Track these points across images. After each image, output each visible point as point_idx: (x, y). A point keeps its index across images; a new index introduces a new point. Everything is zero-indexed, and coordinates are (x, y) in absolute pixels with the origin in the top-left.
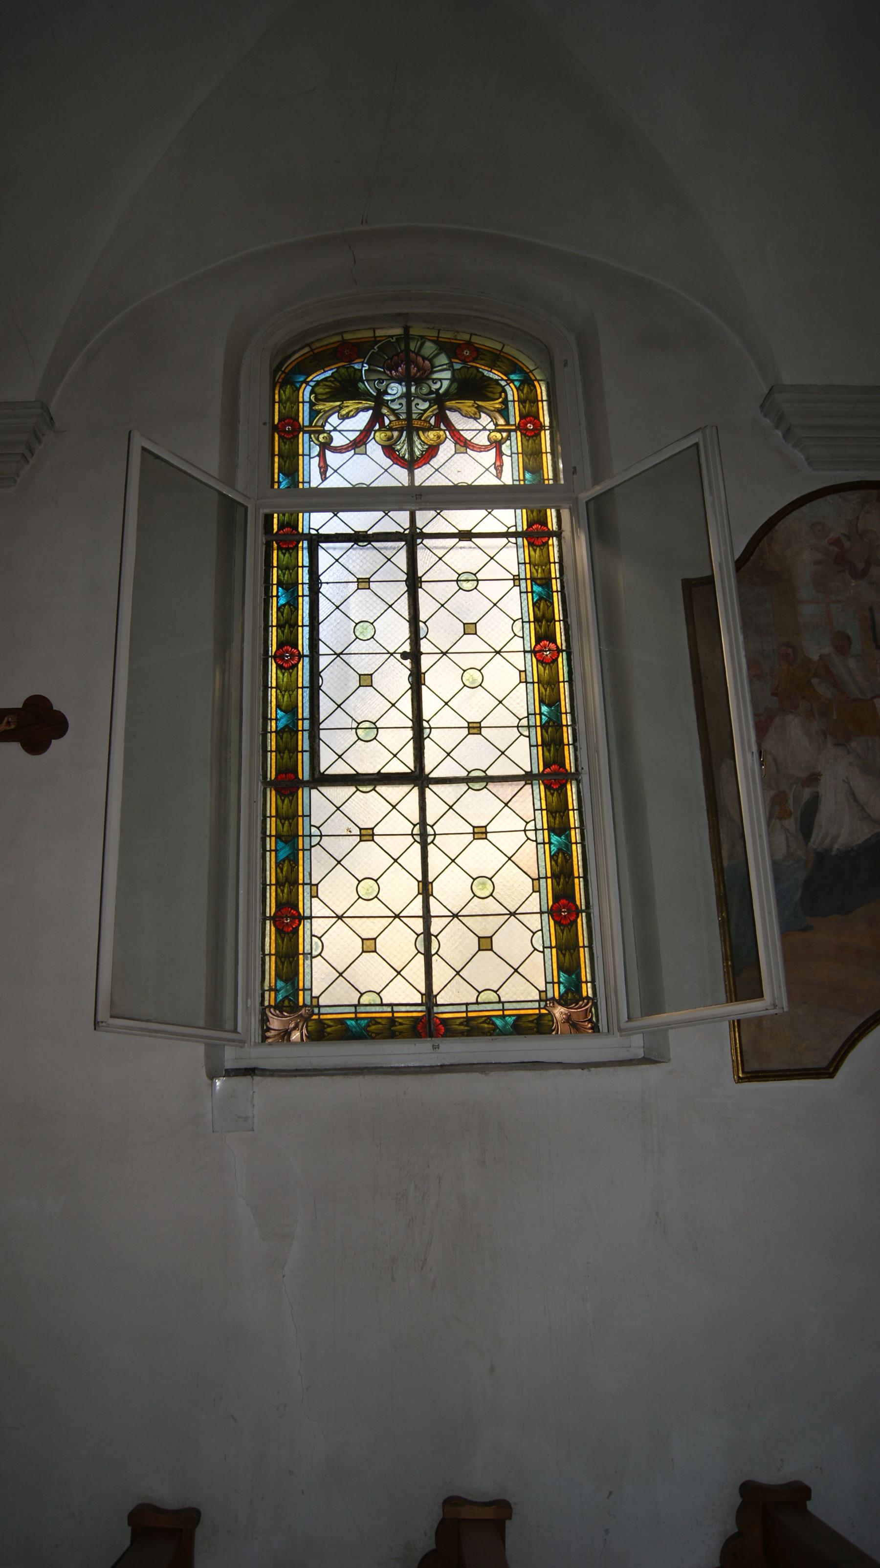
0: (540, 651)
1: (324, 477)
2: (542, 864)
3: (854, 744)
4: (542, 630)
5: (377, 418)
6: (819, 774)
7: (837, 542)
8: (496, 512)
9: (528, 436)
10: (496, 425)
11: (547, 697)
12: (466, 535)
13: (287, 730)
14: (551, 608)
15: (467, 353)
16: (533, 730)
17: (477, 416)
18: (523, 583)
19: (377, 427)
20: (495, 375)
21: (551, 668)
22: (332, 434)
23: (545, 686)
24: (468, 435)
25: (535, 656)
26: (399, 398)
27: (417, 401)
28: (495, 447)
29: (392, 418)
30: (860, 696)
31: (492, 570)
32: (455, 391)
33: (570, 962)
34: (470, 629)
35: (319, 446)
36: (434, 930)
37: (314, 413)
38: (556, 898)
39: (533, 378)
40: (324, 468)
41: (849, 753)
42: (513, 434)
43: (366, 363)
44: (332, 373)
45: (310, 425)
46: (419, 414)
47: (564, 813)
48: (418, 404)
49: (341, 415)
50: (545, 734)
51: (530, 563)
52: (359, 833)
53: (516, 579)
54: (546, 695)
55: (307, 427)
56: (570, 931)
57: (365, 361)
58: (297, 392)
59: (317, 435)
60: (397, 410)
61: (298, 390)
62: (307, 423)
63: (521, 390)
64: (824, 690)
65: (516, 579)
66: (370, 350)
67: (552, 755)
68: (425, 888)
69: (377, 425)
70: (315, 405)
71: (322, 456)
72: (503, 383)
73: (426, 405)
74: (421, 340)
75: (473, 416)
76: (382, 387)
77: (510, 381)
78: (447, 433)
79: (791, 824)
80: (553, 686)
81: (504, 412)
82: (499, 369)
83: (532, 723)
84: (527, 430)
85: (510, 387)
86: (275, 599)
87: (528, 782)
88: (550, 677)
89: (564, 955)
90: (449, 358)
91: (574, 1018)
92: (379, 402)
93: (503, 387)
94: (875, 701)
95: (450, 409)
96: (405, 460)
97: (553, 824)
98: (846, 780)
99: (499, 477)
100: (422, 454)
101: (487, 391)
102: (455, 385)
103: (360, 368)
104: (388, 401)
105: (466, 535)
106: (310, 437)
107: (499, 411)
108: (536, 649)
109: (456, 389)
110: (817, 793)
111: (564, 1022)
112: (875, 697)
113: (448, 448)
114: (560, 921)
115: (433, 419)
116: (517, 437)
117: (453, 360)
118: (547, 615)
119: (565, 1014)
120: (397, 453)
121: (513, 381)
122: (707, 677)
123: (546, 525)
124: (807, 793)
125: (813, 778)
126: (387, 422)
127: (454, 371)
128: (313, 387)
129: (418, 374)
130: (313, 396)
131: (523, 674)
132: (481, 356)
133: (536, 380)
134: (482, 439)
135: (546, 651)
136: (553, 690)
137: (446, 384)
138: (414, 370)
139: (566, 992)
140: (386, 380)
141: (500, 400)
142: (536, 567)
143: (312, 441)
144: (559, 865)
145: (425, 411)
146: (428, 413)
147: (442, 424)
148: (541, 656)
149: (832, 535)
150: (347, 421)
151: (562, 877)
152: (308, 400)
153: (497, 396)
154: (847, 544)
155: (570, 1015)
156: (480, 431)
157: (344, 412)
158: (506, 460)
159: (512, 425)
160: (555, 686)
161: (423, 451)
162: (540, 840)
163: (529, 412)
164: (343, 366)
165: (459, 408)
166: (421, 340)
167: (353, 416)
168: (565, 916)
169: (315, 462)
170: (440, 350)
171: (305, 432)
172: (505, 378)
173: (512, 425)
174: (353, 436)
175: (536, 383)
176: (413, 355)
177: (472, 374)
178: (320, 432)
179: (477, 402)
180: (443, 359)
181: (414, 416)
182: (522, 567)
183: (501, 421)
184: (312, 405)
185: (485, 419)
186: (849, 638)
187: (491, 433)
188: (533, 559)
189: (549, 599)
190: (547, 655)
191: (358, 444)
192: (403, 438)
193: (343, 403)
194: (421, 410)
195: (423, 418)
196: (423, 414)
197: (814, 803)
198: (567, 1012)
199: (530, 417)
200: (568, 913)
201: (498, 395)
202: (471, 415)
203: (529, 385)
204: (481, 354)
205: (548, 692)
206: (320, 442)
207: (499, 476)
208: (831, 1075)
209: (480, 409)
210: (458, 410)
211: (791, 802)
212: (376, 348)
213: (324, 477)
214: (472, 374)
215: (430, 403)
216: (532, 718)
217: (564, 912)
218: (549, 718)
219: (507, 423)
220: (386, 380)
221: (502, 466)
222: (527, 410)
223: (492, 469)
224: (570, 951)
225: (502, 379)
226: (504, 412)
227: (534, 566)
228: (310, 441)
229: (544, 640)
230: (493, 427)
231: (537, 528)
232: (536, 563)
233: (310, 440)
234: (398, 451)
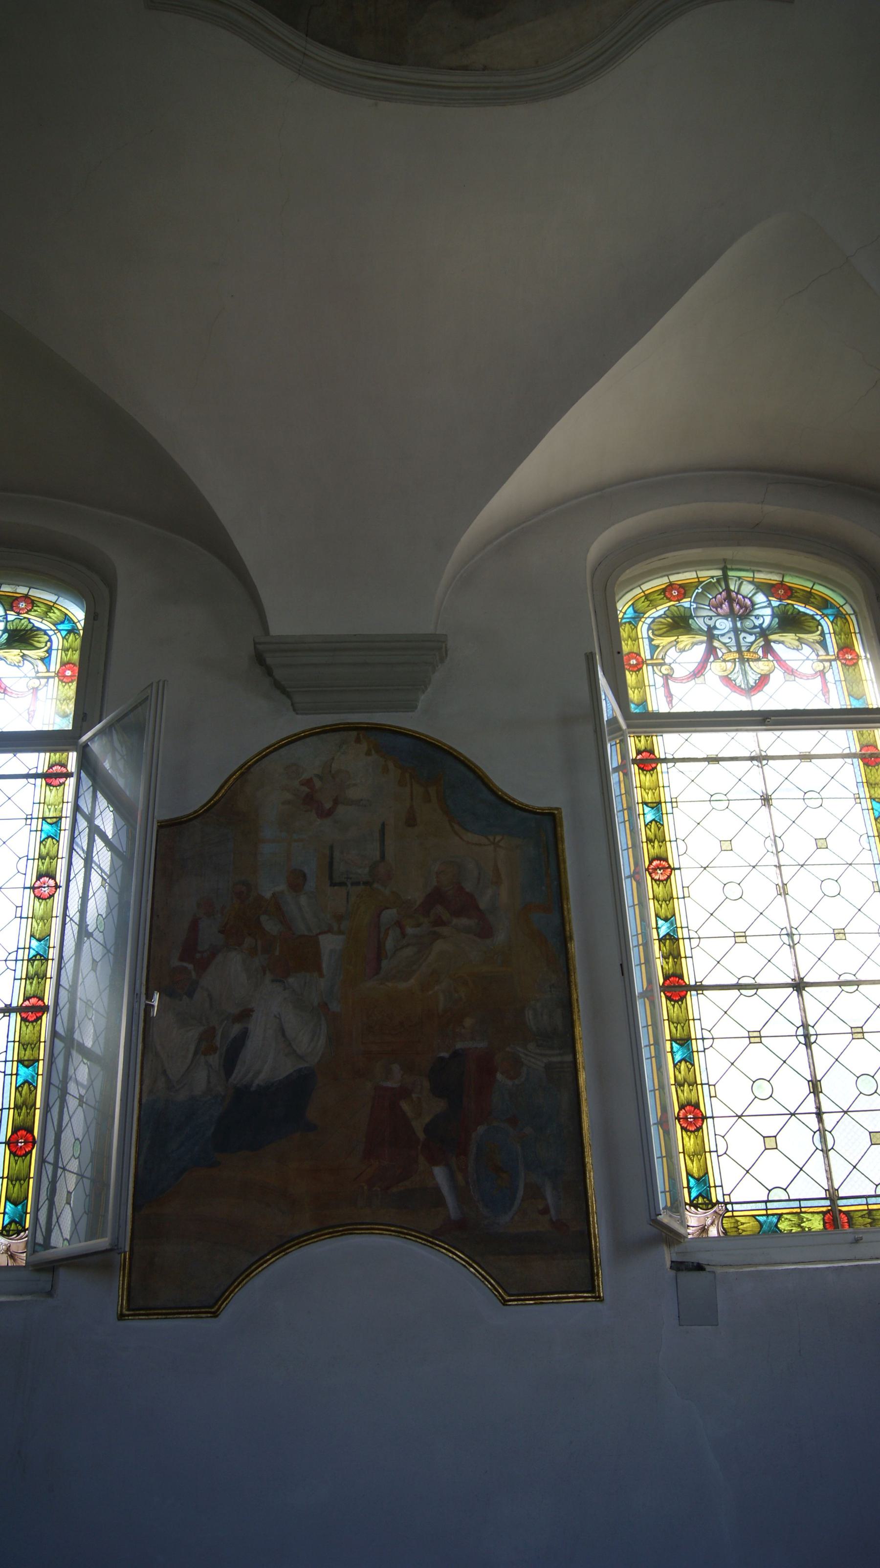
0: (39, 887)
1: (670, 702)
2: (7, 1095)
3: (291, 980)
4: (45, 867)
5: (711, 650)
6: (252, 1010)
7: (308, 783)
8: (19, 755)
9: (64, 682)
10: (818, 655)
11: (38, 932)
12: (806, 757)
13: (668, 937)
14: (56, 846)
15: (22, 605)
16: (19, 963)
17: (21, 664)
18: (863, 801)
19: (712, 659)
20: (810, 611)
21: (47, 903)
22: (672, 665)
23: (38, 921)
24: (793, 665)
25: (34, 892)
26: (728, 632)
27: (743, 635)
28: (820, 675)
29: (724, 651)
30: (306, 933)
31: (741, 791)
32: (777, 626)
33: (18, 1192)
34: (821, 844)
35: (662, 677)
36: (828, 1125)
37: (654, 648)
38: (15, 1130)
39: (844, 612)
40: (669, 696)
41: (285, 989)
42: (833, 663)
43: (693, 602)
44: (665, 612)
45: (652, 658)
46: (748, 646)
47: (35, 1045)
48: (745, 638)
49: (679, 649)
50: (30, 967)
51: (641, 787)
52: (850, 1031)
53: (857, 798)
54: (37, 930)
55: (648, 660)
56: (23, 1162)
57: (692, 601)
58: (635, 629)
59: (659, 667)
60: (728, 643)
61: (636, 627)
62: (648, 657)
63: (66, 639)
64: (270, 926)
65: (29, 818)
66: (695, 591)
67: (33, 988)
68: (815, 1087)
69: (712, 656)
70: (653, 640)
71: (666, 686)
72: (818, 618)
73: (751, 638)
74: (739, 580)
75: (17, 664)
76: (711, 623)
77: (824, 615)
78: (775, 662)
79: (215, 1060)
80: (46, 921)
81: (823, 643)
82: (811, 605)
83: (20, 957)
84: (65, 676)
85: (825, 620)
86: (642, 817)
87: (6, 1014)
88: (44, 912)
89: (14, 1186)
90: (767, 597)
91: (13, 1249)
92: (710, 634)
93: (818, 621)
94: (320, 937)
95: (774, 642)
96: (742, 689)
97: (23, 1056)
98: (278, 1016)
99: (828, 702)
100: (755, 683)
101: (33, 640)
102: (776, 620)
103: (689, 606)
104: (718, 635)
105: (806, 757)
106: (653, 670)
107: (42, 659)
108: (36, 886)
109: (6, 639)
110: (247, 1029)
111: (3, 1253)
112: (320, 934)
113: (777, 676)
114: (16, 1151)
115: (761, 650)
116: (837, 665)
117: (8, 612)
118: (51, 853)
119: (5, 1245)
120: (734, 682)
121: (60, 631)
122: (158, 916)
123: (654, 754)
124: (236, 1029)
125: (245, 1014)
126: (720, 654)
127: (773, 608)
128: (649, 625)
129: (741, 611)
130: (650, 632)
131: (19, 909)
132: (35, 608)
133: (847, 614)
134: (807, 668)
135: (44, 887)
136: (45, 924)
137: (768, 620)
138: (737, 607)
139: (10, 1223)
140: (714, 616)
141: (819, 632)
142: (50, 807)
143: (656, 673)
144: (23, 1095)
145: (752, 643)
146: (754, 646)
147: (769, 655)
148: (39, 892)
149: (305, 776)
150: (684, 653)
151: (24, 1108)
152: (646, 636)
153: (43, 645)
154: (318, 784)
155: (10, 1246)
156: (804, 661)
157: (681, 646)
158: (831, 686)
159: (831, 655)
160: (47, 920)
161: (756, 680)
162: (8, 1072)
163: (845, 643)
164: (673, 605)
165: (5, 657)
166: (739, 580)
167: (689, 649)
168: (21, 1147)
169: (661, 691)
170: (757, 589)
171: (647, 665)
172: (54, 628)
173: (831, 655)
174: (692, 667)
175: (847, 617)
176: (734, 595)
177: (23, 625)
178: (661, 665)
179: (22, 651)
180: (760, 598)
181: (744, 649)
182: (36, 806)
183: (822, 652)
184: (651, 640)
185: (806, 650)
186: (304, 876)
187: (814, 663)
188: (47, 800)
189: (55, 838)
190: (45, 891)
191: (699, 672)
192: (736, 670)
193: (678, 638)
194: (749, 643)
195: (751, 650)
196: (751, 646)
197: (241, 1039)
198: (7, 1243)
199: (846, 648)
200: (24, 1144)
201: (44, 644)
202: (16, 663)
203: (841, 618)
204: (36, 606)
205: (40, 926)
206: (663, 674)
207: (827, 701)
208: (215, 1315)
209: (25, 658)
210: (782, 642)
211: (218, 1038)
212: (699, 588)
213: (670, 702)
214: (23, 625)
215: (756, 637)
216: (21, 952)
217: (21, 1143)
218: (37, 952)
219: (48, 671)
220: (714, 616)
221: (828, 692)
222: (68, 657)
223: (820, 695)
224: (20, 1181)
225: (817, 614)
226: (45, 660)
227: (645, 790)
228: (654, 674)
229: (44, 877)
230: (815, 657)
231: (56, 770)
232: (51, 802)
233: (654, 672)
234: (735, 681)
